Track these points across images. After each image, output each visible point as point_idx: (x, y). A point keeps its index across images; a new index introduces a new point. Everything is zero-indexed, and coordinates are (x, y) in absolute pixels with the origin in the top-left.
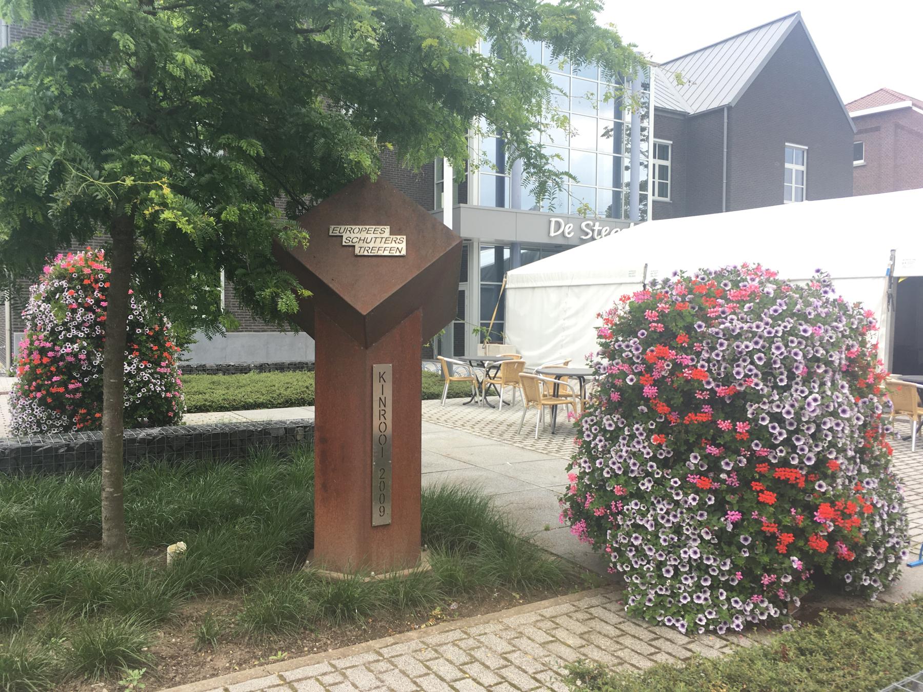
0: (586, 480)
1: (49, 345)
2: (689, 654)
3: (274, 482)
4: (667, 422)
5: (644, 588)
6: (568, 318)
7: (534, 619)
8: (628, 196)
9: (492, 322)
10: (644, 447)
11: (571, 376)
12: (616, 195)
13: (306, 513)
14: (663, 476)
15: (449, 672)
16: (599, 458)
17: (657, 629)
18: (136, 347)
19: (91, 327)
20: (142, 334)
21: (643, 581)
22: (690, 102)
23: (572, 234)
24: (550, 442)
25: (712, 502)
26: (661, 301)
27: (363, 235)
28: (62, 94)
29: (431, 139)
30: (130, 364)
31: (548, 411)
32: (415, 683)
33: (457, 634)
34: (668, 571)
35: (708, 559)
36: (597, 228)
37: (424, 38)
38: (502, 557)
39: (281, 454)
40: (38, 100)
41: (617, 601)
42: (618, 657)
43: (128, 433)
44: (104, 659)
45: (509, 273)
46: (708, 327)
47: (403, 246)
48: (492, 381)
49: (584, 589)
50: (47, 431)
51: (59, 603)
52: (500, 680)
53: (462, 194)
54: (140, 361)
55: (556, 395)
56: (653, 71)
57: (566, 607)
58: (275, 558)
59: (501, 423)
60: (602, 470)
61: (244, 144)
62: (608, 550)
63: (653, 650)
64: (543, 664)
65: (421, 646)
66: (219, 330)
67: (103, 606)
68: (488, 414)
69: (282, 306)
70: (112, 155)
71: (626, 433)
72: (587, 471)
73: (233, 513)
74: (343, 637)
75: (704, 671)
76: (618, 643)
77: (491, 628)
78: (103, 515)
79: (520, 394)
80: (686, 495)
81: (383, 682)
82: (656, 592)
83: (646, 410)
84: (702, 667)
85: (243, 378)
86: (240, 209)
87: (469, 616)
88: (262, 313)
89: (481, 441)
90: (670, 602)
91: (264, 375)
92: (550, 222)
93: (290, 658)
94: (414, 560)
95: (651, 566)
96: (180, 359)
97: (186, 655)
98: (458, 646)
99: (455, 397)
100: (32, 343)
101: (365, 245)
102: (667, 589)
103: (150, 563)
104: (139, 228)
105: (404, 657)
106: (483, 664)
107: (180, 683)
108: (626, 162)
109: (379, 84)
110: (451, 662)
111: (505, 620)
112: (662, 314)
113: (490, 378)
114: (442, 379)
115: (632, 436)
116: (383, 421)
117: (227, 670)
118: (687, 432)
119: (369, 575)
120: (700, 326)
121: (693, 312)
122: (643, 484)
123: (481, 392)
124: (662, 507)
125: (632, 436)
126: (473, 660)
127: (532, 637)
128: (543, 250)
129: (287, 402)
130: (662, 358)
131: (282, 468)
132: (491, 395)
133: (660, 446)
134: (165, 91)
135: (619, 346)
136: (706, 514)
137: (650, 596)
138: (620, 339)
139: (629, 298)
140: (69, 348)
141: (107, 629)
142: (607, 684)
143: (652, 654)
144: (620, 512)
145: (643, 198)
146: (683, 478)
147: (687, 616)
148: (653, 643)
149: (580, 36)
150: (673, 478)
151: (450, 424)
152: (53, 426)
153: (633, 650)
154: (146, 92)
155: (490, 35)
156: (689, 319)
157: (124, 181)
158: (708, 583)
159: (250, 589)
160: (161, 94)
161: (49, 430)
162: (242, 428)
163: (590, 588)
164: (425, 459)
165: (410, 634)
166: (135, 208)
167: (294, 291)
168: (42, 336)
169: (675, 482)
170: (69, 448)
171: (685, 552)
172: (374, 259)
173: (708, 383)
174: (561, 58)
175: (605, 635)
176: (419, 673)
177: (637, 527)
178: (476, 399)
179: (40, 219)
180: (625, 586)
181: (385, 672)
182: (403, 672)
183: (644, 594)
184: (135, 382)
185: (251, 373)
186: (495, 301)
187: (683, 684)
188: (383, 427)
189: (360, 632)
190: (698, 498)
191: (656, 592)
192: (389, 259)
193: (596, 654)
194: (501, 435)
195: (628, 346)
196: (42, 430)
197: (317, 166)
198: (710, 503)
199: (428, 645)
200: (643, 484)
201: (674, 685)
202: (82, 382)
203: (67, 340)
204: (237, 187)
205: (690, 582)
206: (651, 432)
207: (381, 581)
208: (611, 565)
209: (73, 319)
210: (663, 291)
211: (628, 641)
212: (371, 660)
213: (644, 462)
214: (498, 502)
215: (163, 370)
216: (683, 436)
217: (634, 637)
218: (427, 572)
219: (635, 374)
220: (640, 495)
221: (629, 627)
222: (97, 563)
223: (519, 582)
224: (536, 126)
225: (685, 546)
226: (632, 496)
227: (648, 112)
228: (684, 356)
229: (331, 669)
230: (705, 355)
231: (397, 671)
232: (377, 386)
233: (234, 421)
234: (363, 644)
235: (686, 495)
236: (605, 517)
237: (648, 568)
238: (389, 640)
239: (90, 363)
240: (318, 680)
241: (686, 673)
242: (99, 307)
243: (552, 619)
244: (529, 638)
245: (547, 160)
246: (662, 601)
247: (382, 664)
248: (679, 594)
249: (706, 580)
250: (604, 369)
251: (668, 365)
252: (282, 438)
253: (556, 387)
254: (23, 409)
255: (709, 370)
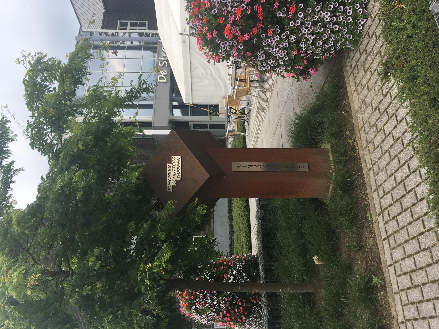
0: (290, 68)
1: (221, 314)
2: (377, 18)
3: (286, 215)
4: (262, 28)
5: (343, 40)
6: (206, 73)
7: (356, 94)
8: (146, 43)
9: (208, 110)
10: (274, 39)
11: (236, 73)
12: (146, 49)
13: (301, 202)
14: (288, 30)
15: (381, 136)
16: (279, 62)
17: (364, 33)
18: (222, 276)
19: (213, 295)
20: (216, 273)
21: (340, 40)
22: (99, 11)
23: (165, 71)
24: (268, 83)
25: (302, 5)
26: (202, 31)
27: (171, 176)
28: (112, 313)
29: (124, 144)
30: (230, 278)
31: (252, 84)
32: (385, 153)
33: (362, 132)
34: (336, 28)
35: (330, 7)
36: (162, 59)
37: (78, 148)
38: (325, 109)
39: (272, 212)
40: (114, 322)
41: (349, 53)
42: (377, 54)
43: (262, 281)
44: (367, 294)
45: (185, 102)
46: (215, 7)
47: (176, 157)
48: (238, 111)
49: (342, 69)
50: (260, 315)
51: (340, 312)
52: (386, 112)
53: (148, 125)
54: (229, 274)
55: (245, 80)
56: (84, 30)
57: (351, 79)
58: (322, 216)
59: (258, 107)
60: (284, 61)
61: (131, 230)
62: (324, 57)
63: (374, 36)
64: (379, 91)
65: (367, 149)
66: (214, 241)
67: (342, 293)
68: (254, 113)
69: (203, 213)
70: (138, 289)
71: (267, 49)
72: (285, 68)
73: (300, 233)
74: (361, 186)
75: (386, 12)
76: (370, 54)
77: (360, 116)
78: (300, 292)
79: (244, 98)
80: (298, 18)
81: (384, 168)
82: (346, 34)
83: (256, 39)
84: (384, 12)
85: (235, 228)
86: (160, 231)
87: (354, 126)
88: (207, 221)
89: (267, 117)
90: (351, 27)
91: (234, 218)
92: (160, 82)
93: (370, 210)
94: (325, 152)
95: (333, 36)
96: (227, 256)
97: (366, 257)
98: (368, 132)
99: (245, 129)
100: (220, 321)
101: (176, 175)
102: (344, 28)
103: (323, 271)
104: (170, 278)
105: (372, 158)
106: (377, 120)
107: (380, 260)
108: (129, 43)
109: (99, 168)
110: (376, 136)
111: (356, 109)
112: (209, 31)
113: (236, 112)
114: (236, 135)
115: (269, 45)
116: (257, 167)
117: (374, 239)
118: (267, 18)
119: (332, 173)
120: (215, 11)
121: (207, 15)
122: (292, 40)
123: (243, 117)
124: (304, 31)
125: (269, 45)
126: (375, 125)
127: (365, 96)
128: (173, 85)
129: (247, 208)
130: (230, 31)
131: (279, 211)
132: (244, 112)
133: (274, 32)
134: (106, 266)
135: (224, 52)
136: (308, 8)
137: (347, 37)
138: (220, 51)
139: (200, 46)
140: (223, 305)
141: (353, 291)
142: (391, 61)
143: (376, 37)
144: (306, 51)
145: (147, 35)
146: (290, 20)
147: (358, 19)
148: (371, 36)
149: (73, 72)
150: (289, 25)
151: (258, 132)
152: (258, 313)
153: (374, 46)
154: (108, 274)
155: (73, 115)
156: (211, 17)
157: (147, 284)
158: (342, 7)
159: (336, 227)
160: (108, 267)
161: (259, 313)
162: (260, 229)
163: (342, 66)
164: (275, 146)
165: (361, 155)
166: (162, 279)
167: (197, 206)
168: (217, 317)
169: (292, 24)
170: (268, 305)
171: (327, 19)
172: (183, 171)
173: (243, 7)
174: (84, 80)
175: (366, 60)
176: (380, 151)
177: (313, 43)
178: (246, 119)
179: (167, 320)
180: (342, 49)
181: (379, 167)
182: (379, 158)
183: (346, 40)
184: (238, 276)
185: (233, 224)
186: (198, 109)
187: (393, 23)
188: (261, 167)
189: (359, 178)
190: (300, 13)
191: (346, 34)
192: (183, 164)
193: (375, 65)
194: (264, 108)
195: (224, 48)
196: (260, 317)
197: (139, 197)
198: (303, 6)
199: (367, 146)
200: (292, 40)
201: (393, 27)
202: (238, 299)
203: (219, 306)
204: (150, 233)
205: (341, 17)
206: (267, 37)
207: (335, 168)
208: (331, 56)
209: (209, 303)
210: (197, 29)
211: (369, 49)
212: (372, 173)
213: (281, 40)
214: (298, 111)
215: (233, 264)
216: (269, 20)
217: (367, 45)
218: (331, 146)
219: (238, 45)
220: (298, 41)
221: (362, 48)
222: (322, 295)
223: (337, 101)
224: (117, 93)
225: (323, 19)
226: (298, 46)
227: (104, 32)
228: (230, 19)
229: (376, 192)
230: (229, 9)
231: (379, 161)
232: (243, 170)
233: (256, 233)
234: (365, 177)
235: (298, 18)
236: (307, 59)
237: (334, 38)
238: (363, 164)
239: (229, 296)
240: (381, 198)
241: (387, 21)
242: (204, 292)
243: (356, 86)
244: (366, 97)
245: (133, 88)
246: (350, 31)
247: (375, 168)
248: (347, 22)
249: (341, 9)
250: (235, 59)
251: (234, 28)
252: (265, 211)
253: (241, 80)
254: (250, 325)
255: (237, 7)
